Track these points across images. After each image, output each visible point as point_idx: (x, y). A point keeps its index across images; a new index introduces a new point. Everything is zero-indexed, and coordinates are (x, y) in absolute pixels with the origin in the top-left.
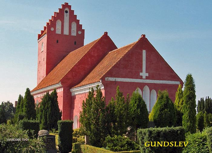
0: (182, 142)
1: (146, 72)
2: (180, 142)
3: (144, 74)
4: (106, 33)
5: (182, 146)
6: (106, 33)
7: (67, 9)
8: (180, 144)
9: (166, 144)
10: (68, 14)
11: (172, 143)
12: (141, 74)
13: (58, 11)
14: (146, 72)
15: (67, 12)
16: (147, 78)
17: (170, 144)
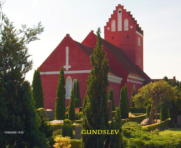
0: (114, 130)
1: (69, 65)
2: (112, 130)
3: (67, 67)
5: (114, 134)
6: (68, 35)
7: (120, 10)
8: (112, 132)
9: (100, 132)
11: (105, 131)
12: (65, 67)
14: (69, 65)
15: (120, 12)
16: (70, 69)
17: (103, 132)
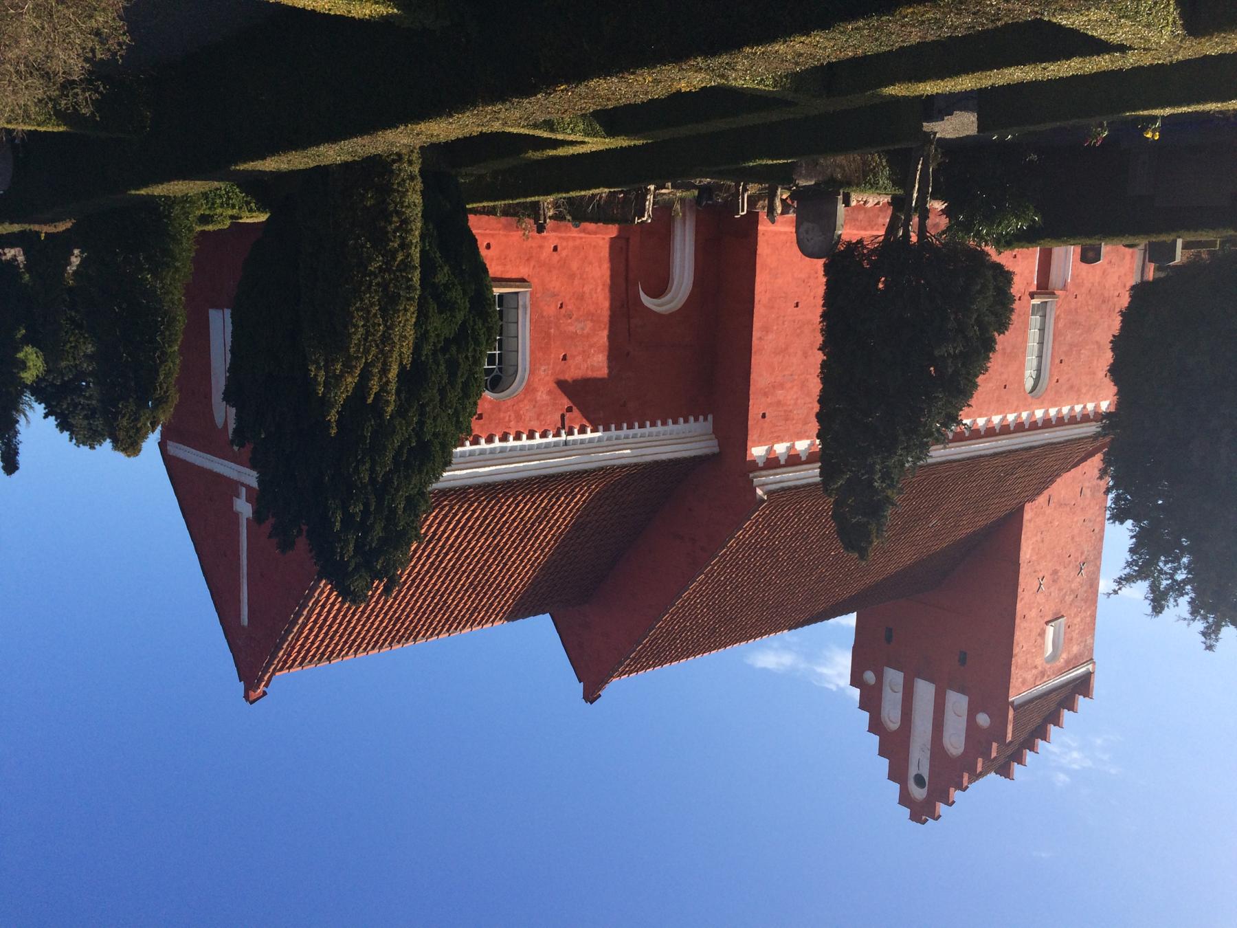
4: (591, 695)
7: (919, 793)
10: (913, 771)
13: (956, 795)
15: (919, 781)
